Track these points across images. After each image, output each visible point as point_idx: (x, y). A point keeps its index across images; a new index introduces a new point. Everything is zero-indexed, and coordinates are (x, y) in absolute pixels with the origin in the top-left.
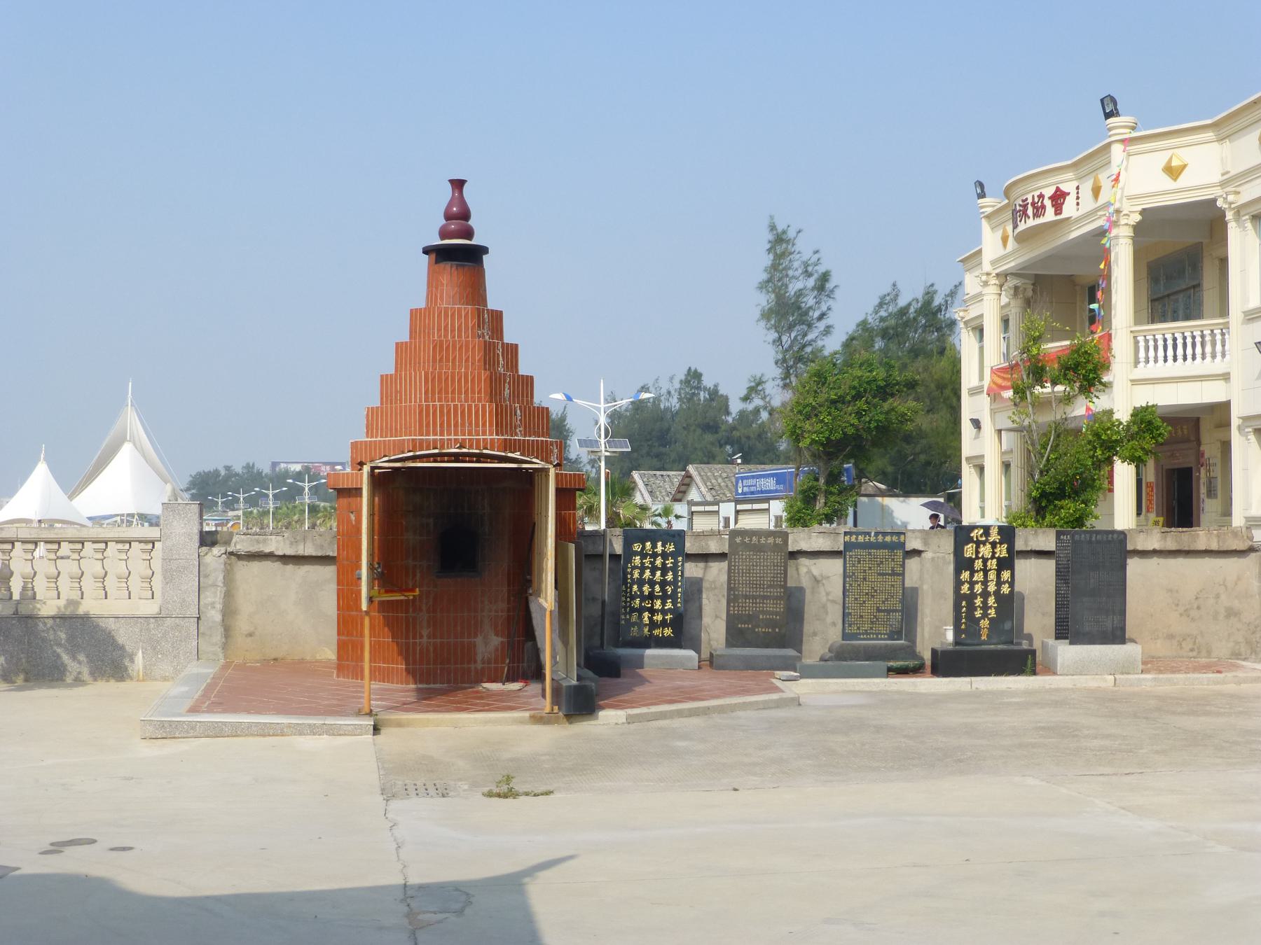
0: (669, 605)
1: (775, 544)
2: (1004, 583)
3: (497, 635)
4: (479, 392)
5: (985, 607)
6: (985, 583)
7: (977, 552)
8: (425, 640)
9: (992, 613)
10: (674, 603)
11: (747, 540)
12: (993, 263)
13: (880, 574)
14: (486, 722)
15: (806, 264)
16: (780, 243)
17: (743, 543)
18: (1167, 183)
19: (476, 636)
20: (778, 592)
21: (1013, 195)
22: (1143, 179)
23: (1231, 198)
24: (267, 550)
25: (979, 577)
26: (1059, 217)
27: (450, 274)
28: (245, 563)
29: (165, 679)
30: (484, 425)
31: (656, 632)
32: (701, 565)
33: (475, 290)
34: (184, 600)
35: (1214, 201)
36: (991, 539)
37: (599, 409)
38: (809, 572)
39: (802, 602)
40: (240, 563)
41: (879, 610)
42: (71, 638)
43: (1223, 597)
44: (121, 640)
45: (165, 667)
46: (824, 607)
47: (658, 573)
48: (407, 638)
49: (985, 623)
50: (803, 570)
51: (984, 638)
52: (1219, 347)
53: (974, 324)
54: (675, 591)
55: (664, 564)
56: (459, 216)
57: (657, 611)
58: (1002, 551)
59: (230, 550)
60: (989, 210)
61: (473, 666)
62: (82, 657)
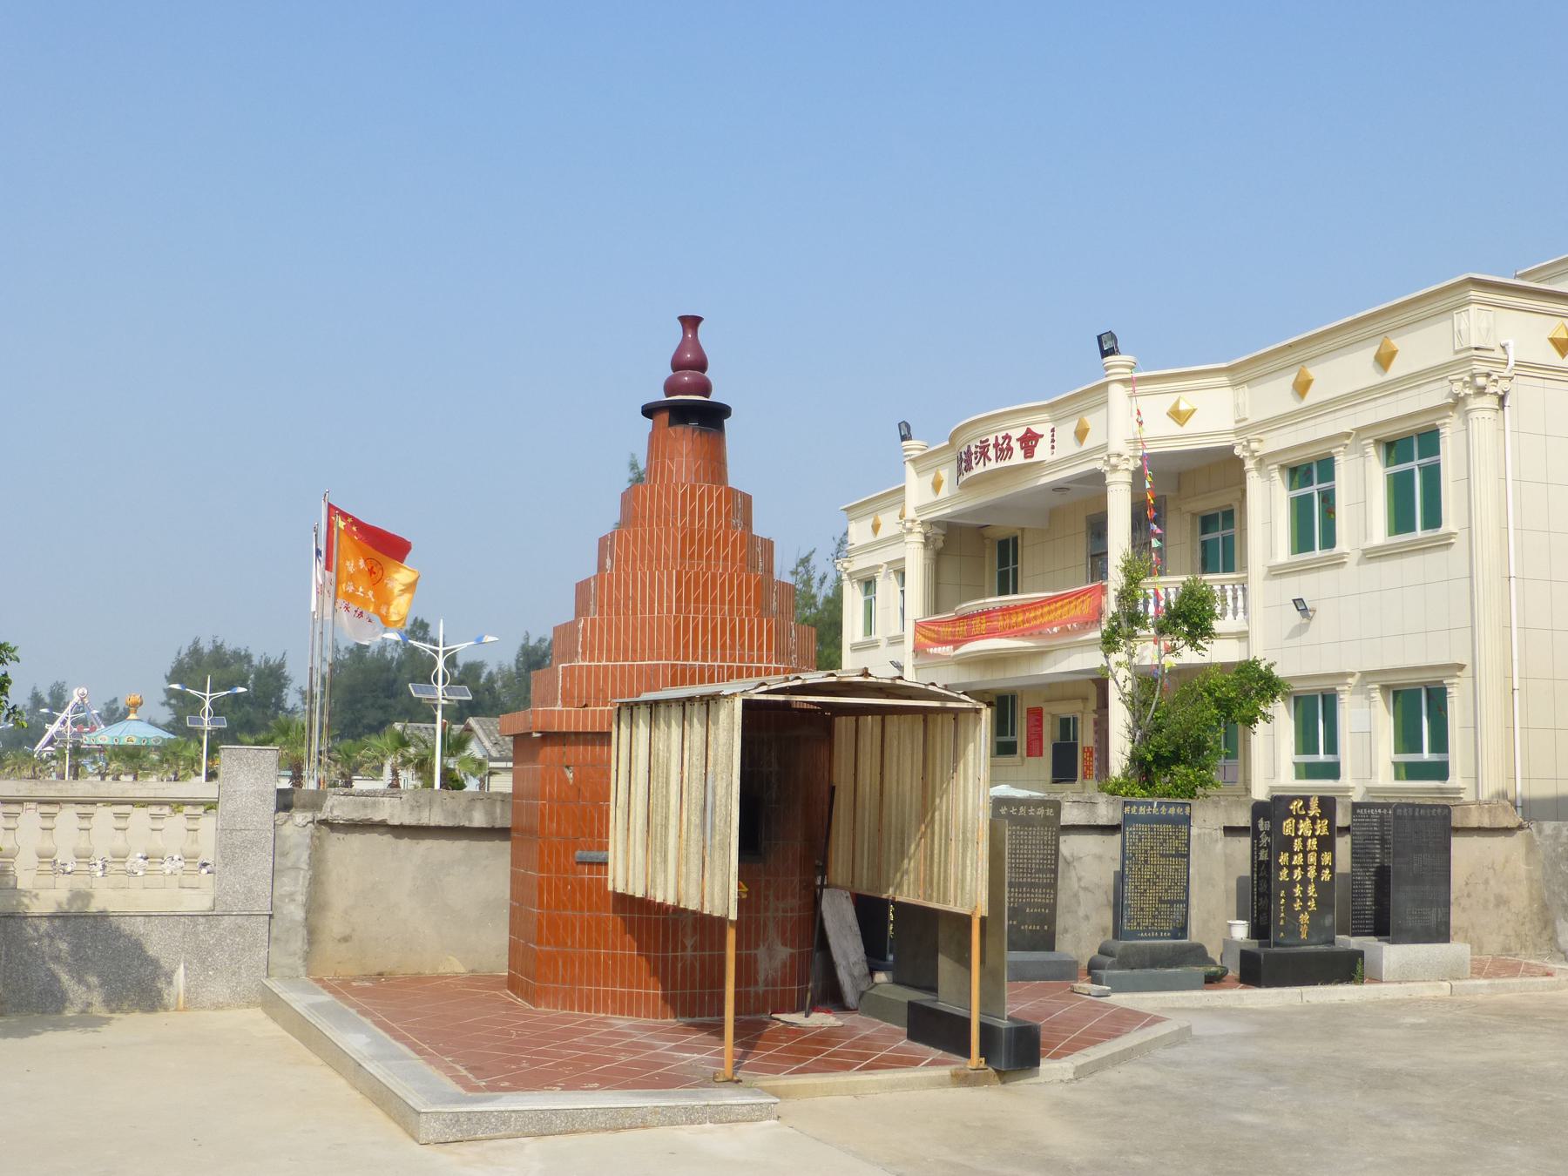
2: (1325, 867)
3: (785, 944)
4: (748, 603)
5: (1305, 899)
6: (1305, 867)
7: (1297, 829)
8: (689, 952)
9: (1312, 904)
12: (918, 509)
13: (1162, 856)
14: (893, 1086)
17: (1009, 816)
18: (1173, 428)
19: (757, 946)
21: (959, 442)
22: (1130, 426)
23: (1254, 446)
24: (377, 818)
25: (1298, 860)
27: (685, 439)
28: (341, 836)
29: (218, 1007)
30: (760, 647)
33: (715, 466)
34: (250, 890)
35: (1232, 448)
36: (1311, 813)
37: (437, 652)
40: (335, 835)
41: (1161, 901)
42: (76, 950)
43: (1492, 882)
44: (152, 951)
45: (219, 989)
46: (1076, 895)
48: (665, 950)
49: (1304, 918)
51: (1304, 936)
52: (1240, 603)
56: (690, 363)
58: (1322, 828)
59: (320, 816)
60: (917, 453)
61: (752, 989)
62: (93, 980)
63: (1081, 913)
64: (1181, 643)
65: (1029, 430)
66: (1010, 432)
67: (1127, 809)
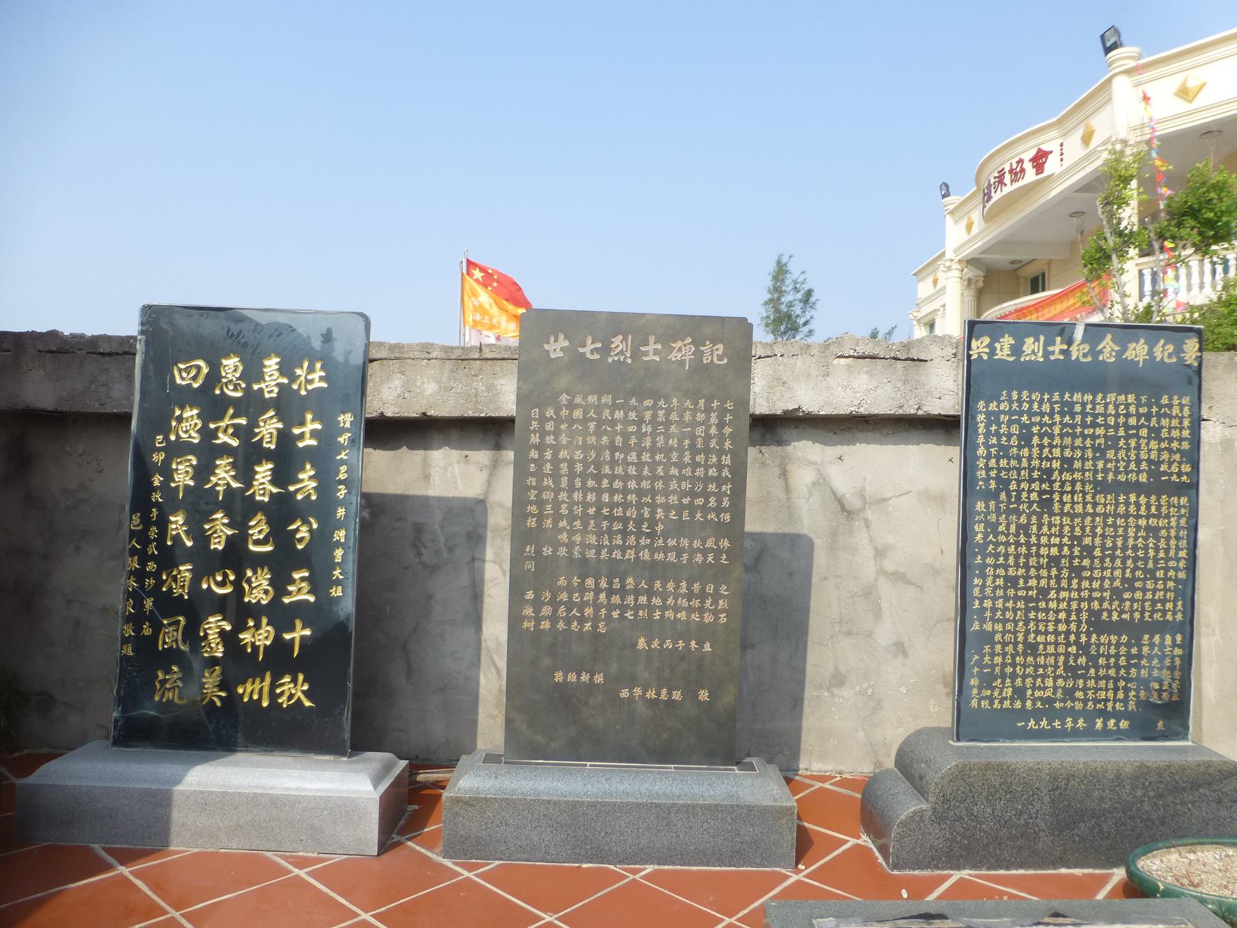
0: (300, 592)
1: (700, 369)
10: (318, 584)
11: (589, 349)
12: (956, 251)
13: (1101, 487)
15: (795, 282)
16: (781, 272)
18: (1182, 106)
20: (700, 549)
26: (1040, 176)
31: (249, 690)
32: (482, 456)
38: (822, 483)
39: (802, 578)
41: (1098, 624)
46: (869, 592)
47: (264, 471)
50: (802, 477)
53: (925, 320)
54: (322, 539)
55: (285, 438)
57: (255, 611)
60: (951, 207)
63: (885, 634)
64: (1190, 251)
65: (1040, 150)
66: (1022, 156)
67: (980, 347)
